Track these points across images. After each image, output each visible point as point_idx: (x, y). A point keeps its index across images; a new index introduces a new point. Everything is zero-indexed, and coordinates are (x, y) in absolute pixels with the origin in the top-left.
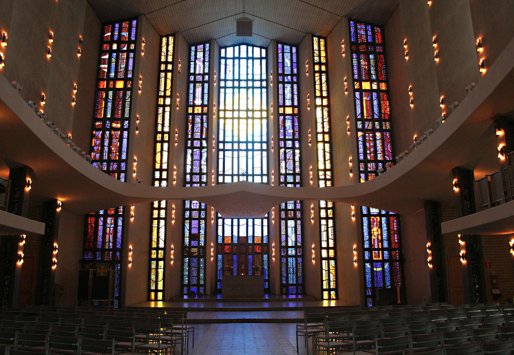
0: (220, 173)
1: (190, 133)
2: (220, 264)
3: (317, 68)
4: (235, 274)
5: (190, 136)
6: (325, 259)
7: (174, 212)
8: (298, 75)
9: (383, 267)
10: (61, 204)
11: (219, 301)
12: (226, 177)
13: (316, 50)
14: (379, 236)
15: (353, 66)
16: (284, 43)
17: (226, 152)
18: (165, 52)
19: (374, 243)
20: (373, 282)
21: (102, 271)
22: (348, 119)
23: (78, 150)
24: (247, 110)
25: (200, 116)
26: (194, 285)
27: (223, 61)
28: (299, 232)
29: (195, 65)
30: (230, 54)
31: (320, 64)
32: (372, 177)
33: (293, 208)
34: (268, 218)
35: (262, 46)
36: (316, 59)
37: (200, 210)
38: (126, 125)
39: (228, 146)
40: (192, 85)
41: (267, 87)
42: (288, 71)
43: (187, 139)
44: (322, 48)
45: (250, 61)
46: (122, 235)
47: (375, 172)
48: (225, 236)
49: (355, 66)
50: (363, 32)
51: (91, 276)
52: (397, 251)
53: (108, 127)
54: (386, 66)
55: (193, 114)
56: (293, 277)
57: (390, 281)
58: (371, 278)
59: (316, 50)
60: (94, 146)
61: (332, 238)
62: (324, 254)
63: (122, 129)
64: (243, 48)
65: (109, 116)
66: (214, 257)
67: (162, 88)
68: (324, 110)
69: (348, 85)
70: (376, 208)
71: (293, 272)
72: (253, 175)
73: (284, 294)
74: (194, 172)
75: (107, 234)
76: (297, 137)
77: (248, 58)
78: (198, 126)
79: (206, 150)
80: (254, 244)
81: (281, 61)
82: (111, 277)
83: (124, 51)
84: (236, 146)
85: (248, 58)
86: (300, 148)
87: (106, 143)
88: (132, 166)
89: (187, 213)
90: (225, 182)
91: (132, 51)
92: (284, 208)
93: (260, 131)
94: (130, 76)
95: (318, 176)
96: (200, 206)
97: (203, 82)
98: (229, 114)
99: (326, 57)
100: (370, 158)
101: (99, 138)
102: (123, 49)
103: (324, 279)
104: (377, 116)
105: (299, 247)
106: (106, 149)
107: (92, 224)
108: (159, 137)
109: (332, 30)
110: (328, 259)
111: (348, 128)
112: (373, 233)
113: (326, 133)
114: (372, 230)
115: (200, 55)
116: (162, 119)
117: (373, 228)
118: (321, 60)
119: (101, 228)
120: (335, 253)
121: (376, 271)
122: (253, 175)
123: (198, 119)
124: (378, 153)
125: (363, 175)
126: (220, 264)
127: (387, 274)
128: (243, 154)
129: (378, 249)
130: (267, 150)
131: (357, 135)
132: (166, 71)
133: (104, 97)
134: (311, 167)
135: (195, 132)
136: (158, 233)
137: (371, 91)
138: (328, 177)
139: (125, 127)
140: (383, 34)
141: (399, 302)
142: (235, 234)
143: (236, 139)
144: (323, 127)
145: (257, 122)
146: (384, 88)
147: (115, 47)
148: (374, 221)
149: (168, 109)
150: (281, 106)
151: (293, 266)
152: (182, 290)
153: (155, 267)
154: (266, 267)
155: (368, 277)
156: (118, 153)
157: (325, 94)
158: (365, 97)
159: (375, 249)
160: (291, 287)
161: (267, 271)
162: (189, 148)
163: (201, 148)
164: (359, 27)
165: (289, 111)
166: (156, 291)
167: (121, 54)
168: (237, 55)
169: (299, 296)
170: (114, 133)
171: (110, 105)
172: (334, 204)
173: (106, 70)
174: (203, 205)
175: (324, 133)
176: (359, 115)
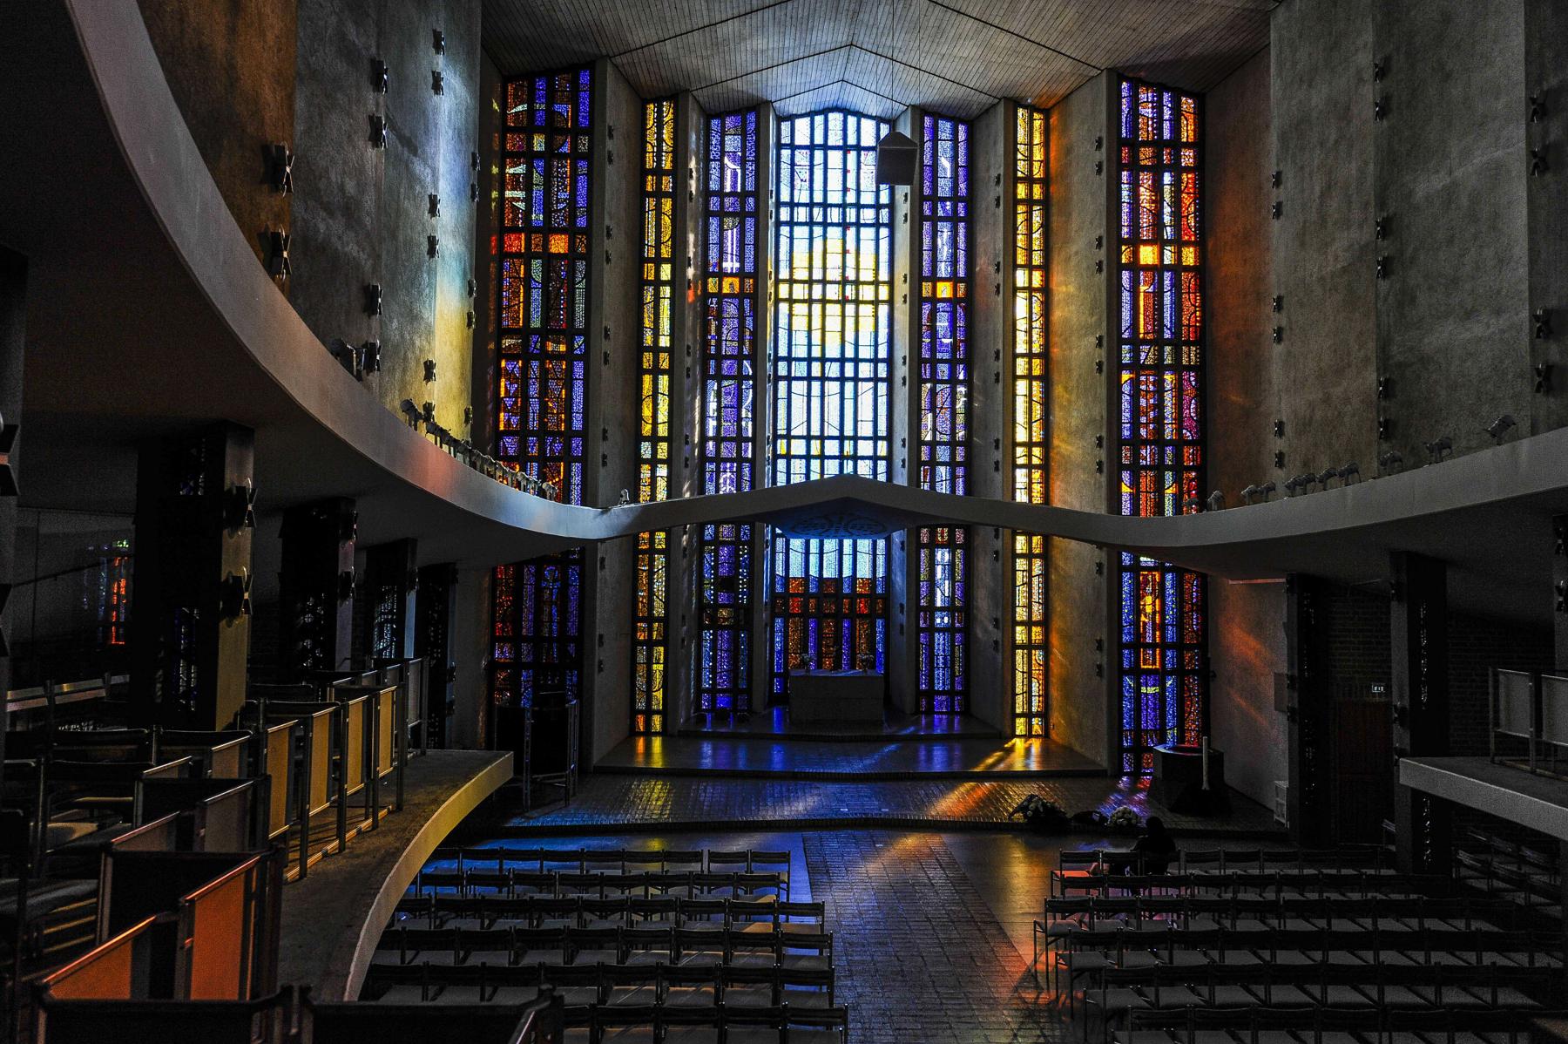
0: (779, 432)
3: (1021, 191)
6: (1022, 647)
17: (794, 383)
19: (1145, 632)
24: (844, 282)
29: (722, 168)
30: (802, 138)
35: (883, 115)
36: (1022, 166)
39: (799, 369)
42: (944, 187)
44: (1037, 139)
55: (720, 295)
56: (944, 675)
64: (835, 119)
65: (536, 323)
68: (1034, 299)
76: (960, 355)
77: (845, 149)
78: (731, 325)
83: (565, 156)
86: (968, 382)
87: (534, 390)
94: (581, 222)
97: (741, 215)
99: (1046, 162)
103: (1018, 690)
109: (1072, 93)
115: (732, 143)
116: (652, 316)
117: (1144, 597)
121: (1146, 694)
123: (731, 309)
125: (1126, 476)
129: (1153, 646)
132: (659, 194)
133: (522, 276)
137: (1158, 269)
142: (813, 572)
144: (1030, 342)
147: (539, 143)
148: (1146, 582)
149: (666, 291)
150: (927, 279)
151: (944, 651)
156: (563, 416)
157: (1037, 259)
158: (1144, 285)
159: (1147, 646)
164: (1143, 97)
165: (944, 290)
166: (649, 713)
168: (819, 140)
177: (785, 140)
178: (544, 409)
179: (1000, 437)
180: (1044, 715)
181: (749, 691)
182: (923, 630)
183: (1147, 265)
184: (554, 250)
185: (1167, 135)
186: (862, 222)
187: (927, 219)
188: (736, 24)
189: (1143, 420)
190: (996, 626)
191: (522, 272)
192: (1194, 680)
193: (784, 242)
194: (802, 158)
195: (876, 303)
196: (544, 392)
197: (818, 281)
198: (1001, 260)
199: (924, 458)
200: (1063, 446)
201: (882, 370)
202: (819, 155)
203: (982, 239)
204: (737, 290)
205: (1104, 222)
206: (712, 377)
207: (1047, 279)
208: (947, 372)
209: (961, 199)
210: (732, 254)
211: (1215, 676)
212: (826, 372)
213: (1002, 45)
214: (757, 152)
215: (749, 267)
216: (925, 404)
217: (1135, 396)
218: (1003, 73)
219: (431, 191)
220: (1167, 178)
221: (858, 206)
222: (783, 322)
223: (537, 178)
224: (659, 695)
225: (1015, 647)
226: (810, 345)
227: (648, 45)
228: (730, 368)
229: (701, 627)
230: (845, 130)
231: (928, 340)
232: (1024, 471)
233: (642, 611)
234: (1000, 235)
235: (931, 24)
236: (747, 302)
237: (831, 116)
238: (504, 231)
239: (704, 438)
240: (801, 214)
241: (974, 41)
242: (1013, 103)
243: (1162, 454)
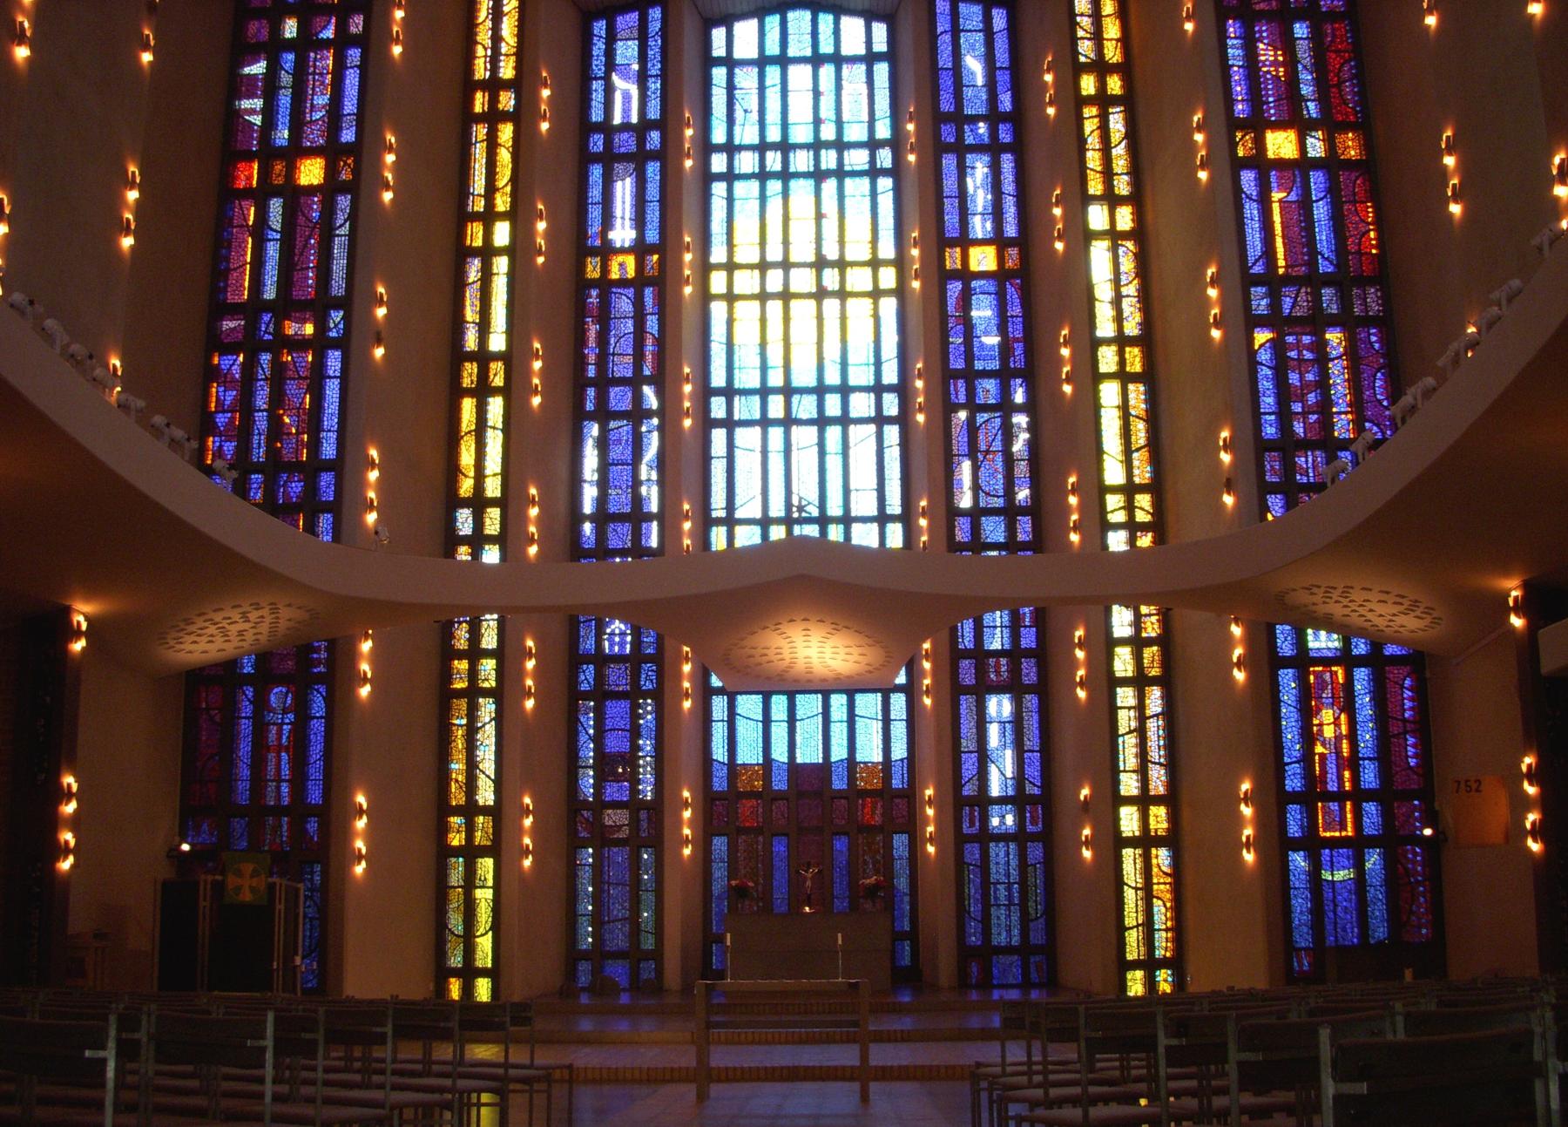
0: (714, 514)
1: (592, 358)
2: (719, 872)
3: (1088, 85)
4: (780, 905)
5: (591, 372)
6: (1132, 842)
7: (530, 664)
8: (1017, 117)
10: (84, 626)
13: (1082, 15)
14: (1344, 741)
15: (1225, 68)
18: (488, 43)
21: (246, 884)
22: (1212, 278)
23: (133, 406)
24: (820, 264)
25: (631, 292)
26: (619, 955)
27: (719, 74)
28: (1032, 740)
29: (609, 90)
31: (1101, 68)
33: (1007, 647)
36: (1086, 48)
37: (635, 660)
38: (336, 326)
39: (747, 408)
40: (596, 172)
41: (896, 172)
42: (975, 102)
43: (580, 383)
45: (827, 71)
49: (1236, 69)
51: (204, 904)
52: (1416, 802)
53: (267, 337)
57: (1388, 921)
58: (1311, 911)
59: (1082, 15)
60: (217, 412)
61: (1162, 760)
62: (1129, 822)
63: (320, 344)
65: (270, 293)
66: (693, 842)
67: (479, 185)
68: (1121, 251)
69: (1209, 143)
71: (1010, 897)
72: (847, 520)
73: (977, 986)
74: (612, 509)
75: (268, 749)
76: (1018, 359)
77: (816, 60)
79: (655, 421)
81: (950, 65)
82: (280, 907)
83: (326, 44)
84: (776, 407)
87: (262, 399)
88: (362, 483)
89: (588, 674)
91: (356, 41)
92: (970, 646)
93: (872, 345)
94: (348, 136)
95: (1103, 511)
96: (637, 643)
98: (746, 282)
99: (1125, 41)
100: (1305, 432)
101: (234, 380)
102: (321, 36)
103: (1130, 920)
104: (1331, 263)
105: (1033, 800)
106: (261, 421)
107: (213, 713)
110: (1146, 841)
111: (1213, 312)
112: (1321, 732)
113: (1132, 341)
115: (627, 51)
116: (478, 303)
117: (1319, 710)
118: (1106, 51)
119: (245, 726)
120: (1173, 818)
123: (623, 304)
124: (1334, 410)
126: (719, 872)
127: (1376, 893)
128: (804, 437)
129: (1340, 796)
130: (903, 420)
131: (1251, 340)
132: (493, 117)
133: (251, 223)
134: (1072, 479)
135: (613, 354)
137: (1303, 164)
138: (1141, 517)
139: (333, 334)
144: (1119, 319)
145: (859, 309)
146: (1353, 153)
149: (501, 264)
152: (571, 973)
155: (1300, 904)
157: (1122, 186)
158: (1280, 190)
159: (1328, 797)
160: (1003, 959)
161: (907, 899)
162: (592, 417)
163: (638, 414)
167: (312, 55)
168: (773, 49)
169: (1033, 992)
170: (289, 358)
171: (273, 250)
173: (257, 120)
174: (649, 639)
175: (1121, 341)
176: (1257, 261)
186: (847, 168)
187: (948, 148)
191: (252, 218)
209: (1005, 118)
216: (960, 441)
224: (485, 944)
230: (815, 34)
233: (457, 797)
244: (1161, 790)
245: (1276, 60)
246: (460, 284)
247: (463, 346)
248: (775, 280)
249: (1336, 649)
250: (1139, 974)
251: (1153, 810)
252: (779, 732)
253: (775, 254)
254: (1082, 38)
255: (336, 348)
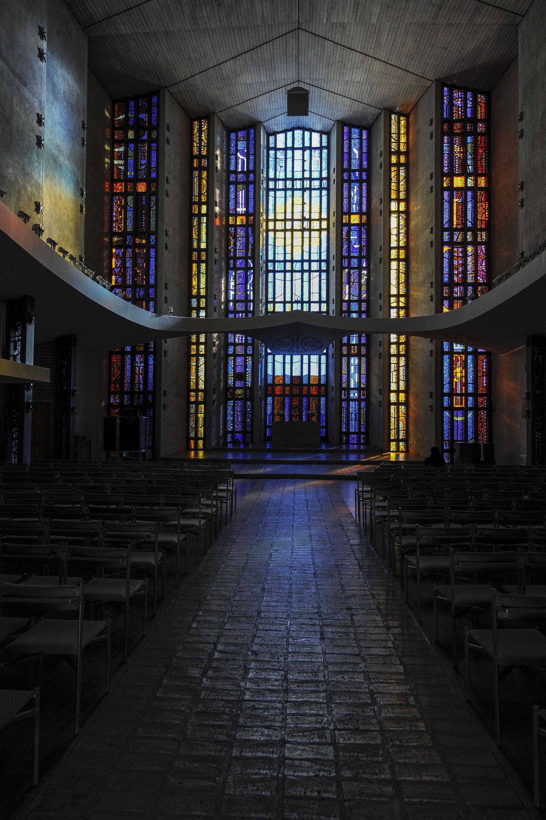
0: (269, 300)
3: (394, 159)
6: (394, 404)
9: (466, 416)
11: (270, 451)
12: (277, 305)
13: (393, 134)
16: (352, 125)
20: (452, 434)
24: (303, 219)
28: (363, 371)
29: (237, 158)
30: (280, 144)
32: (459, 304)
34: (327, 354)
35: (323, 130)
36: (394, 146)
37: (246, 345)
38: (153, 241)
39: (279, 266)
44: (402, 131)
46: (154, 376)
47: (464, 299)
48: (276, 375)
49: (446, 155)
50: (459, 103)
54: (489, 153)
55: (235, 226)
56: (355, 424)
64: (298, 133)
65: (130, 229)
70: (461, 344)
71: (355, 418)
72: (309, 302)
73: (345, 444)
75: (136, 374)
76: (364, 253)
77: (304, 149)
80: (309, 385)
83: (144, 141)
85: (304, 149)
86: (368, 268)
90: (276, 310)
94: (153, 175)
95: (390, 303)
96: (246, 340)
99: (407, 143)
100: (458, 280)
108: (195, 255)
109: (418, 102)
112: (456, 375)
114: (455, 372)
116: (197, 232)
117: (456, 368)
122: (309, 302)
123: (241, 232)
124: (468, 273)
125: (446, 303)
129: (461, 395)
131: (442, 249)
132: (200, 169)
136: (197, 371)
137: (465, 189)
140: (489, 105)
141: (482, 459)
142: (288, 373)
143: (288, 257)
144: (398, 241)
149: (204, 219)
150: (346, 214)
151: (355, 411)
153: (194, 412)
154: (323, 412)
157: (402, 196)
159: (457, 395)
165: (355, 219)
166: (196, 439)
168: (289, 144)
172: (407, 339)
176: (446, 223)
177: (272, 145)
178: (135, 275)
179: (382, 292)
180: (406, 440)
181: (252, 432)
182: (344, 400)
183: (458, 187)
184: (139, 190)
185: (469, 115)
186: (313, 187)
187: (346, 181)
188: (232, 63)
189: (456, 272)
190: (380, 393)
192: (484, 413)
193: (271, 199)
194: (280, 155)
195: (320, 230)
196: (135, 264)
197: (289, 220)
198: (382, 197)
199: (344, 309)
200: (415, 293)
201: (324, 266)
202: (289, 153)
203: (374, 190)
204: (244, 223)
205: (434, 164)
206: (232, 269)
207: (407, 206)
208: (356, 263)
209: (364, 170)
210: (242, 204)
211: (495, 410)
212: (294, 268)
213: (377, 70)
214: (255, 149)
215: (251, 210)
216: (345, 279)
217: (451, 260)
218: (380, 90)
219: (38, 111)
220: (469, 139)
221: (311, 179)
222: (271, 242)
223: (131, 153)
224: (201, 430)
225: (390, 404)
226: (285, 254)
227: (186, 79)
228: (241, 263)
229: (227, 399)
230: (303, 139)
231: (346, 246)
232: (395, 310)
233: (193, 386)
234: (382, 183)
235: (337, 59)
236: (250, 229)
237: (296, 132)
238: (113, 181)
239: (227, 301)
240: (280, 185)
241: (361, 69)
242: (390, 111)
243: (466, 290)
244: (403, 389)
245: (460, 151)
246: (191, 226)
247: (193, 247)
248: (289, 225)
249: (462, 349)
250: (394, 443)
251: (401, 394)
252: (288, 366)
253: (289, 216)
254: (393, 142)
255: (153, 248)
